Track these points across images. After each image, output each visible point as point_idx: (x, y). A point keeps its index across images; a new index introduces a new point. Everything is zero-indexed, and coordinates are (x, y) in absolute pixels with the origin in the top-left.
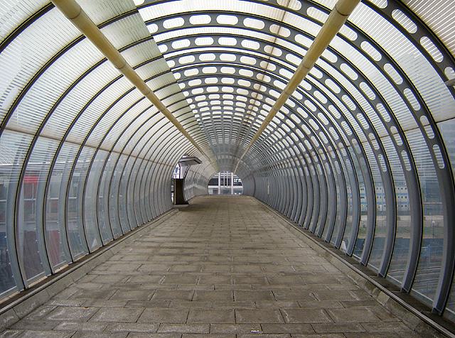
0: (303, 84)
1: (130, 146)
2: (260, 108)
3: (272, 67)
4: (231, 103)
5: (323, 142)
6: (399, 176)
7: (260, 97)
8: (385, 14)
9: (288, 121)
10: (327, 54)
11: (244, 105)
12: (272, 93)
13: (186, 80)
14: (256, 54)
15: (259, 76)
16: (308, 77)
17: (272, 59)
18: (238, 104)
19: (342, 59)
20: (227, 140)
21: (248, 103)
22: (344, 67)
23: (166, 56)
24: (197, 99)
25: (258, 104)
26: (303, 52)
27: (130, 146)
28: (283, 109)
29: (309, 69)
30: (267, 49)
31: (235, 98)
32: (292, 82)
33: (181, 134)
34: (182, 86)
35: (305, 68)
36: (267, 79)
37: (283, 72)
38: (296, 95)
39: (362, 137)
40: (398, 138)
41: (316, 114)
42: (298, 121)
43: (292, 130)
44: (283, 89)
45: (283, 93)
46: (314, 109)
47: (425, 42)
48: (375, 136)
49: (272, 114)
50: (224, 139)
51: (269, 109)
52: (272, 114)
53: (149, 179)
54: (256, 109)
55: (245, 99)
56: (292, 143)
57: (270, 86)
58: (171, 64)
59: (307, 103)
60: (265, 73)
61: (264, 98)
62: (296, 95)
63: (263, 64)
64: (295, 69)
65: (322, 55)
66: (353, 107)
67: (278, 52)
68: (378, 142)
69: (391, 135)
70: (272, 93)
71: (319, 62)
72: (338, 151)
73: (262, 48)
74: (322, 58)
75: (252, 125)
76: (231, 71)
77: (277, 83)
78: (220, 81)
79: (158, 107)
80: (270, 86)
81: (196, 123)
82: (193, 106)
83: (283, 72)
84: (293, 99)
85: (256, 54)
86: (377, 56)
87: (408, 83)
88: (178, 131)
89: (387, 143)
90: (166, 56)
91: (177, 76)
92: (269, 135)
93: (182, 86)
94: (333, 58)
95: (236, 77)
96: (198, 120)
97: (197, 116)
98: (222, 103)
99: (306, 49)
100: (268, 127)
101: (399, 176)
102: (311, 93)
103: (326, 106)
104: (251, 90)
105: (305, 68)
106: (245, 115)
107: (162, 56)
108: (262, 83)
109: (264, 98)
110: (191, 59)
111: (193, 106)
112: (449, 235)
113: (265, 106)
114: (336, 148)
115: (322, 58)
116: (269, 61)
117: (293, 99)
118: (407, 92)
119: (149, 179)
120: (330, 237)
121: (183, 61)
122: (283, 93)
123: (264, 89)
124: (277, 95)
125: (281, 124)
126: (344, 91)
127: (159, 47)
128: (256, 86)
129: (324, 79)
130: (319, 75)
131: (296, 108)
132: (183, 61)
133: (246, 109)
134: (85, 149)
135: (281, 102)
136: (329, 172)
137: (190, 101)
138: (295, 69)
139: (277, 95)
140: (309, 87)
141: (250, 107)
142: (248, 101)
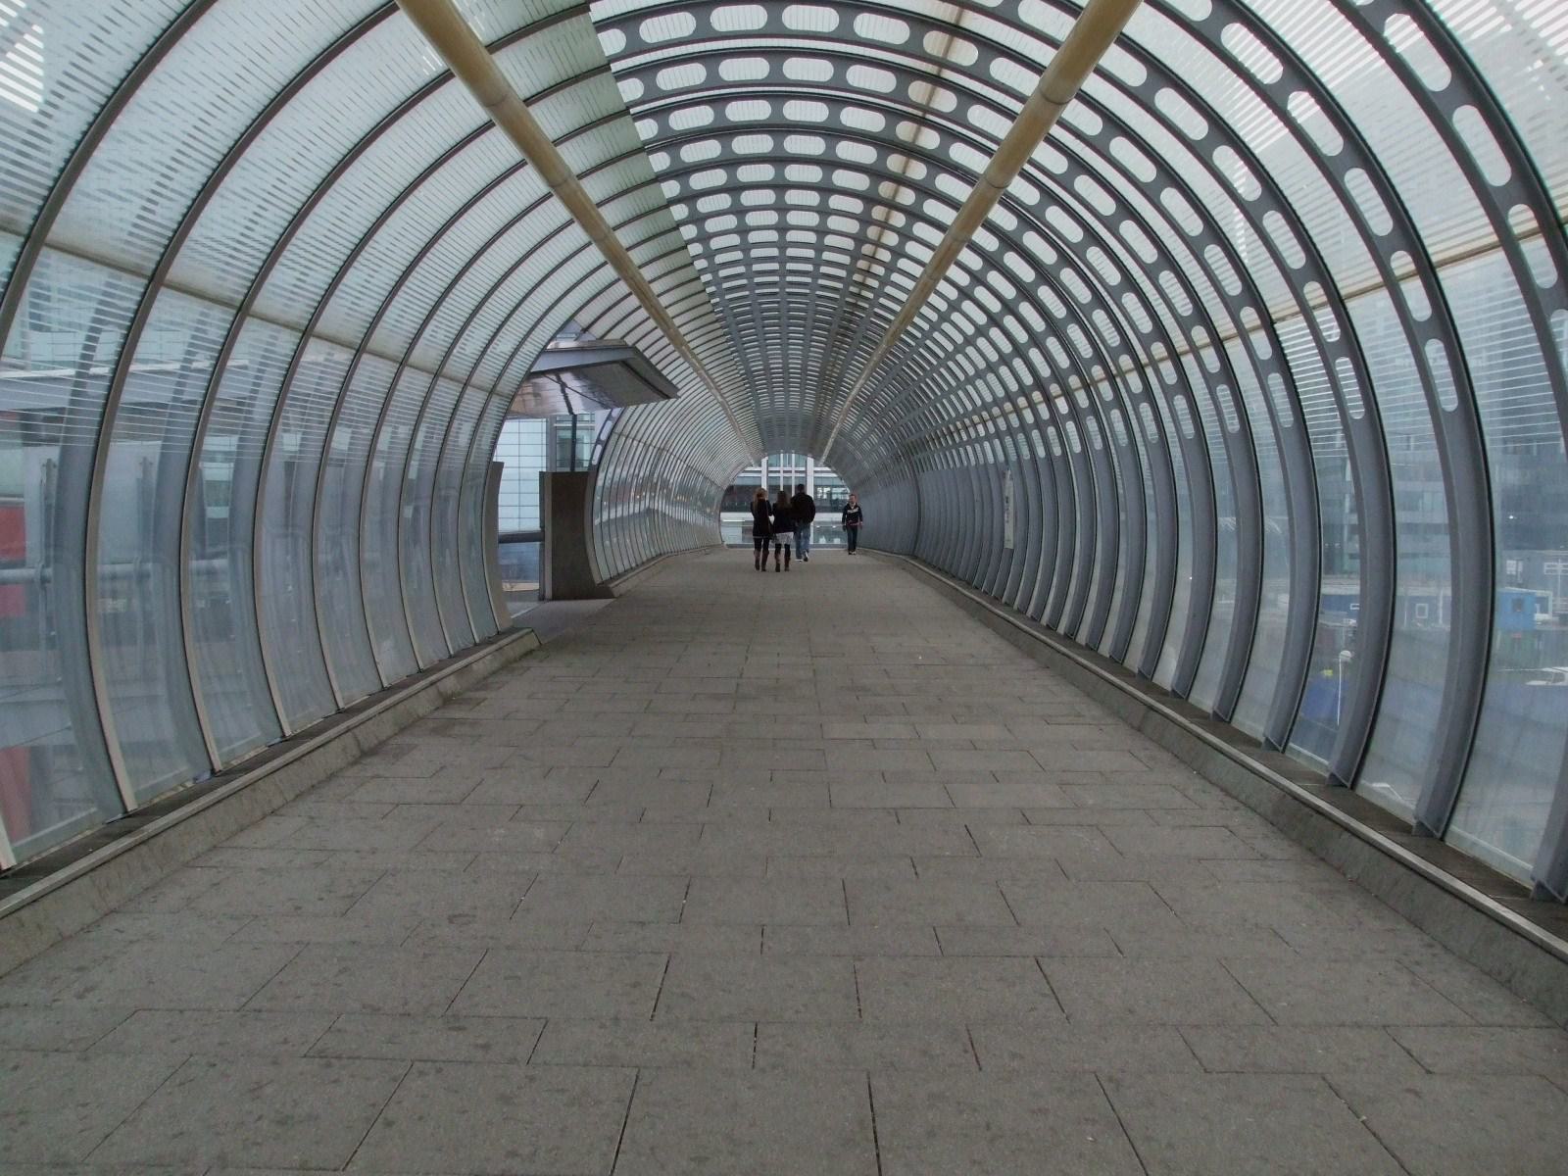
0: (1043, 153)
1: (438, 333)
2: (906, 235)
3: (946, 101)
5: (1103, 342)
6: (1331, 445)
7: (907, 197)
8: (1205, 35)
10: (1115, 59)
11: (849, 244)
12: (946, 183)
13: (672, 142)
15: (904, 131)
16: (1056, 131)
17: (948, 74)
19: (1162, 74)
20: (795, 399)
21: (865, 220)
23: (615, 67)
24: (704, 205)
25: (891, 239)
26: (1045, 55)
27: (438, 333)
28: (967, 256)
29: (1061, 103)
30: (933, 42)
31: (824, 201)
32: (901, 318)
33: (666, 341)
34: (660, 161)
35: (1052, 100)
36: (930, 140)
37: (978, 115)
38: (1020, 189)
39: (1224, 324)
40: (1326, 318)
41: (1080, 249)
43: (1036, 340)
44: (949, 223)
45: (981, 184)
46: (1074, 233)
48: (1328, 292)
49: (945, 257)
50: (787, 397)
51: (936, 237)
52: (945, 257)
54: (885, 256)
55: (853, 226)
56: (1007, 348)
57: (938, 162)
58: (632, 89)
59: (1054, 215)
60: (922, 122)
61: (919, 202)
62: (1020, 189)
63: (917, 91)
64: (1016, 107)
66: (1194, 226)
67: (966, 54)
68: (1338, 317)
69: (1306, 311)
70: (932, 208)
71: (1093, 85)
72: (1149, 371)
73: (916, 38)
74: (1064, 125)
75: (873, 303)
76: (817, 113)
77: (960, 153)
78: (780, 173)
79: (586, 227)
80: (938, 162)
81: (703, 297)
82: (689, 232)
83: (978, 115)
84: (1011, 204)
87: (1471, 84)
88: (651, 323)
89: (1294, 333)
90: (615, 67)
91: (647, 129)
92: (935, 327)
93: (660, 161)
94: (1134, 73)
96: (709, 290)
97: (701, 264)
99: (1020, 98)
100: (925, 310)
101: (1331, 445)
103: (1111, 225)
104: (876, 173)
105: (1052, 100)
106: (850, 273)
107: (605, 68)
108: (912, 151)
109: (909, 225)
110: (695, 74)
111: (689, 232)
113: (921, 229)
114: (1143, 359)
115: (1064, 125)
116: (937, 81)
117: (1011, 204)
118: (1468, 121)
120: (1190, 670)
121: (668, 79)
122: (981, 184)
123: (918, 171)
124: (947, 215)
125: (960, 300)
126: (1169, 176)
127: (602, 36)
128: (895, 162)
129: (1151, 87)
130: (1092, 124)
131: (1040, 208)
132: (668, 79)
133: (855, 255)
134: (252, 335)
136: (1123, 440)
137: (680, 212)
138: (1016, 107)
139: (961, 191)
140: (1058, 164)
141: (872, 232)
142: (863, 230)
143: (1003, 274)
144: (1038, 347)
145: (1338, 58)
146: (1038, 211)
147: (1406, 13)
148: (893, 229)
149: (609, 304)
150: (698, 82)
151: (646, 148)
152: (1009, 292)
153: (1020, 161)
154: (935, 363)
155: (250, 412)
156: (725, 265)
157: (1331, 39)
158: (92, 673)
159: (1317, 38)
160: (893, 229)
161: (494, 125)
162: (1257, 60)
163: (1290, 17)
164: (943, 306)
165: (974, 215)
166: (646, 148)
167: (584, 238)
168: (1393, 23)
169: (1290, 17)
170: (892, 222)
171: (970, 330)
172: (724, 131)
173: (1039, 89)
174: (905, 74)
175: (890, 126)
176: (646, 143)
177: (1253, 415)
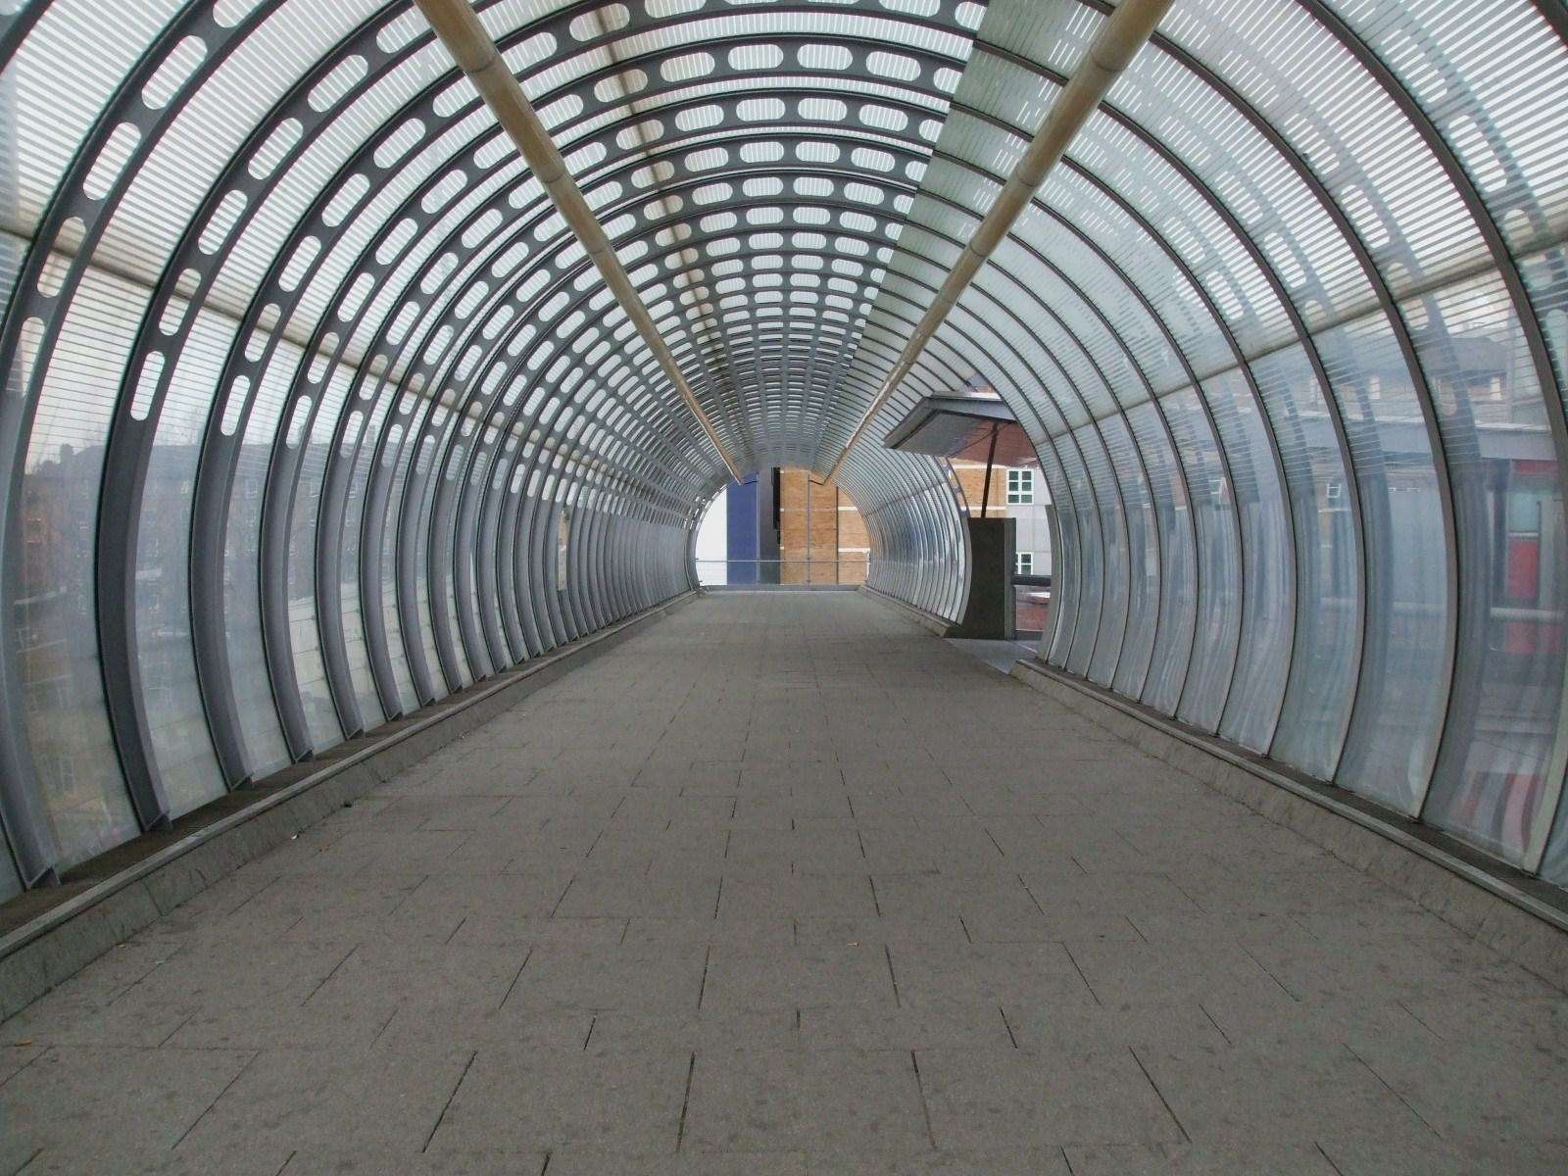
4: (813, 298)
9: (578, 347)
14: (497, 297)
18: (830, 300)
22: (384, 156)
35: (554, 178)
42: (547, 348)
43: (554, 390)
47: (157, 94)
49: (637, 314)
52: (637, 314)
53: (851, 404)
54: (686, 298)
59: (524, 294)
65: (504, 135)
74: (658, 321)
84: (581, 267)
85: (497, 297)
86: (290, 131)
95: (740, 205)
98: (747, 265)
102: (536, 247)
105: (554, 178)
112: (135, 553)
115: (658, 321)
119: (851, 404)
135: (614, 277)
143: (530, 356)
144: (845, 209)
145: (193, 136)
146: (557, 274)
147: (141, 95)
148: (684, 290)
149: (942, 377)
150: (618, 196)
151: (918, 191)
152: (593, 334)
153: (578, 230)
154: (656, 403)
155: (1247, 449)
156: (829, 322)
157: (1272, 167)
158: (1442, 739)
159: (1257, 168)
160: (684, 290)
161: (605, 286)
162: (405, 137)
163: (235, 93)
164: (739, 284)
165: (614, 277)
166: (918, 191)
167: (955, 309)
168: (154, 104)
169: (235, 93)
170: (695, 280)
171: (625, 371)
172: (537, 380)
173: (565, 170)
174: (622, 175)
175: (640, 217)
176: (901, 223)
177: (319, 476)
